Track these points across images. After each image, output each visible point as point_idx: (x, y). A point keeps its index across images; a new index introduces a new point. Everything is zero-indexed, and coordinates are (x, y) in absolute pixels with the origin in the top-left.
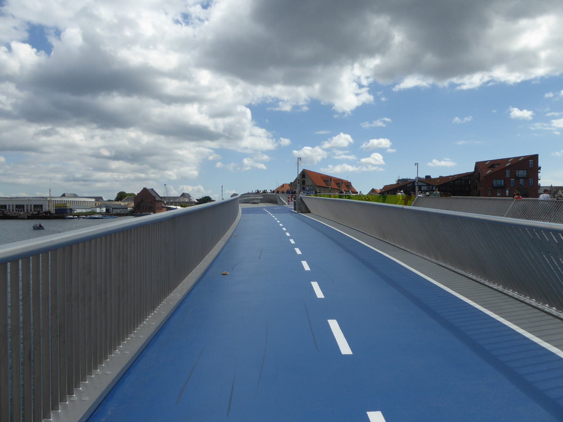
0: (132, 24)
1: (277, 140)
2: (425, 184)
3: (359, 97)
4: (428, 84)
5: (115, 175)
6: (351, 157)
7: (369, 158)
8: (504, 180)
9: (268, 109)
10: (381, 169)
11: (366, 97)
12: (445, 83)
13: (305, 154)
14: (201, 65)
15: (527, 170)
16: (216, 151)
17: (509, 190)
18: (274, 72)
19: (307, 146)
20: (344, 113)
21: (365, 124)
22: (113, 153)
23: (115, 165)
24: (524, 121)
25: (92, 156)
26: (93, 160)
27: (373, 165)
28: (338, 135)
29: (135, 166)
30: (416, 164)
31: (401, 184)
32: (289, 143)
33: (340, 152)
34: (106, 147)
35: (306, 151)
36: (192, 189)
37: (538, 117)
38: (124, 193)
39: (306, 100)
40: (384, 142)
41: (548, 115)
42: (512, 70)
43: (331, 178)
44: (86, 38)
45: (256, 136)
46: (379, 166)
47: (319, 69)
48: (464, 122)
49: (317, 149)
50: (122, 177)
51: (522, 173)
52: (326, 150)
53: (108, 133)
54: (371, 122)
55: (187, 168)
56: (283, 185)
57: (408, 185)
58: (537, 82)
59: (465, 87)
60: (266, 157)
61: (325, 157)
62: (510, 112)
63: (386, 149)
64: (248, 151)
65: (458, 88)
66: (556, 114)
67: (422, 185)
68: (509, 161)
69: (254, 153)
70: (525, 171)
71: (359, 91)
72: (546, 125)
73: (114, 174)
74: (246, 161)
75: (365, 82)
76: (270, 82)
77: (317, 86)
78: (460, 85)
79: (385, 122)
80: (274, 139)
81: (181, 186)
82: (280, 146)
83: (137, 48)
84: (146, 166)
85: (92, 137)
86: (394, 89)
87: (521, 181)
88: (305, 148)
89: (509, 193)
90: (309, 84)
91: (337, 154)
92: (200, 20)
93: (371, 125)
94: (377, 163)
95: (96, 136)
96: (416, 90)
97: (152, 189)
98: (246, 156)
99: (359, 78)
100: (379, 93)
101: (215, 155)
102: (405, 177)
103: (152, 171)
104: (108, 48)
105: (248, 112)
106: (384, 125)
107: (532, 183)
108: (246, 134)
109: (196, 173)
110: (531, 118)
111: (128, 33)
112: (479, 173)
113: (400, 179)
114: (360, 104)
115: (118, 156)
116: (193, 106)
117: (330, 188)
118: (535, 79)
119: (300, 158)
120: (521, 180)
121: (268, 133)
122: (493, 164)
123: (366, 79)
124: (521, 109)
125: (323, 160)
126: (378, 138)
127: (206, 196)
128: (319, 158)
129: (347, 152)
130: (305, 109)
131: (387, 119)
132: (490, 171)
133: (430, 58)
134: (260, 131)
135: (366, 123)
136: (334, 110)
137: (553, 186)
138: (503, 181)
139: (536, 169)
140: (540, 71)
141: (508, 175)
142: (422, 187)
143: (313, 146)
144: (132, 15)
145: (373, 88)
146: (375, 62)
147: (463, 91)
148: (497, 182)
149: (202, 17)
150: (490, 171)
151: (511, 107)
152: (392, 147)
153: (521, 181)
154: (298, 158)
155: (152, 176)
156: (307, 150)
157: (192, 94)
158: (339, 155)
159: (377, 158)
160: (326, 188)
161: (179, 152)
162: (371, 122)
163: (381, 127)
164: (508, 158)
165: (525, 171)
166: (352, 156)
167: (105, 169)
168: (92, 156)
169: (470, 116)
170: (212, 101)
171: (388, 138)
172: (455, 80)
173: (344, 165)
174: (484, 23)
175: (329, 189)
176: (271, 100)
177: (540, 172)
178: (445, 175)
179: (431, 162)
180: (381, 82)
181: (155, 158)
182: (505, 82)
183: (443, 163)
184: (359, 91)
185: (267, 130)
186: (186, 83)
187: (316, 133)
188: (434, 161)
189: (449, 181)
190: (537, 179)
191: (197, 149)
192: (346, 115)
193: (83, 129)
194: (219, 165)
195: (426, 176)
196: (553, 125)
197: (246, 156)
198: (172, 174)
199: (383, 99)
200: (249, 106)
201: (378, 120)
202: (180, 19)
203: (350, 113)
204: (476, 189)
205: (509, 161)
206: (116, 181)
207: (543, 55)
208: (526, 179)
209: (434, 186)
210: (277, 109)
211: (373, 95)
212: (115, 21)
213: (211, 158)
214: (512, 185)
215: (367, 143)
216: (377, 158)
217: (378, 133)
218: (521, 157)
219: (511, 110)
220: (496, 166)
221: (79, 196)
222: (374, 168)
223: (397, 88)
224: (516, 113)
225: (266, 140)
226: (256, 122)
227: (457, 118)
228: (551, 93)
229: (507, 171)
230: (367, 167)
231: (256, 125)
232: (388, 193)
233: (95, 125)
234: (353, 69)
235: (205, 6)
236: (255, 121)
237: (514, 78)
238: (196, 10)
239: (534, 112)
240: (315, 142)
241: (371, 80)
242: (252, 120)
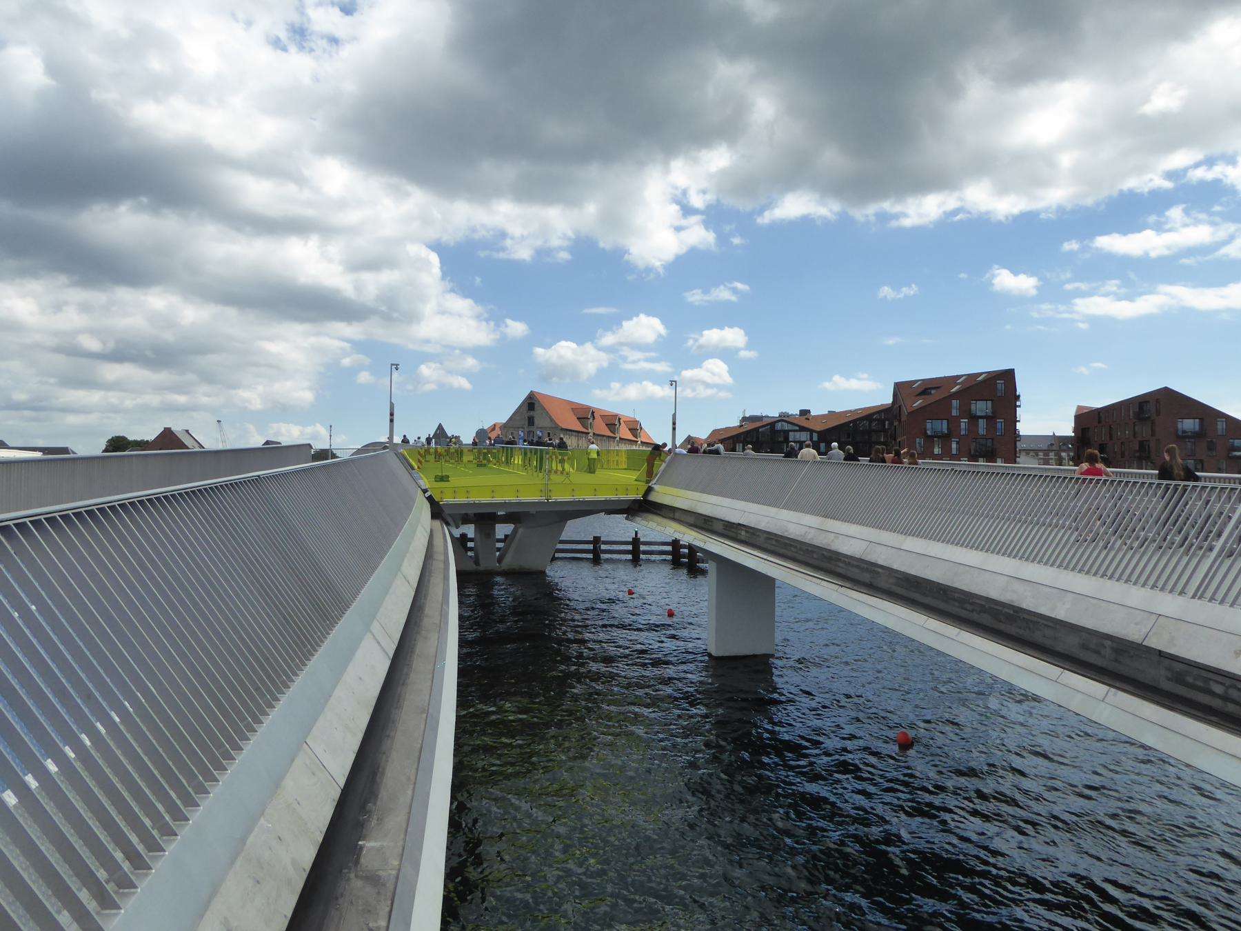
0: (162, 43)
1: (497, 325)
2: (797, 428)
3: (683, 234)
4: (831, 211)
5: (113, 398)
6: (662, 367)
7: (699, 369)
9: (482, 254)
10: (723, 394)
11: (699, 235)
12: (871, 209)
13: (560, 357)
14: (323, 149)
15: (992, 400)
16: (358, 346)
17: (958, 443)
18: (488, 169)
19: (566, 341)
20: (649, 269)
21: (694, 294)
22: (111, 345)
23: (112, 372)
24: (1021, 300)
25: (58, 350)
26: (61, 360)
27: (707, 385)
28: (635, 319)
29: (163, 376)
30: (671, 381)
31: (749, 426)
32: (526, 333)
33: (637, 355)
34: (93, 332)
35: (562, 352)
36: (299, 433)
37: (1049, 292)
38: (124, 438)
39: (565, 237)
40: (733, 336)
41: (1069, 287)
42: (1003, 189)
43: (593, 413)
44: (53, 69)
45: (451, 314)
46: (719, 387)
47: (593, 171)
48: (901, 296)
49: (588, 346)
50: (129, 403)
51: (981, 407)
52: (609, 350)
53: (97, 297)
54: (706, 291)
55: (289, 384)
56: (495, 425)
57: (760, 430)
58: (1050, 215)
59: (907, 223)
60: (470, 362)
61: (605, 364)
62: (994, 276)
63: (737, 350)
64: (430, 349)
65: (894, 224)
66: (1083, 286)
67: (790, 428)
69: (446, 353)
70: (989, 403)
71: (684, 222)
72: (1062, 308)
73: (111, 394)
74: (425, 370)
75: (697, 201)
76: (483, 193)
77: (592, 208)
78: (896, 217)
79: (735, 291)
80: (492, 324)
81: (275, 425)
82: (504, 337)
83: (178, 103)
84: (190, 377)
85: (58, 307)
86: (759, 220)
87: (982, 423)
88: (563, 343)
89: (959, 449)
90: (572, 202)
91: (630, 359)
92: (334, 41)
93: (707, 298)
94: (717, 380)
95: (66, 303)
96: (805, 222)
97: (187, 431)
98: (426, 358)
99: (685, 192)
100: (727, 228)
101: (356, 356)
103: (205, 388)
104: (106, 95)
105: (434, 258)
106: (734, 298)
108: (429, 308)
109: (308, 396)
110: (1034, 292)
111: (156, 64)
112: (900, 407)
114: (682, 250)
115: (121, 353)
116: (306, 242)
117: (591, 434)
118: (1047, 210)
119: (397, 365)
120: (981, 421)
121: (479, 309)
122: (927, 387)
123: (701, 195)
124: (1015, 272)
125: (600, 371)
126: (722, 328)
128: (592, 368)
129: (653, 354)
130: (564, 256)
131: (739, 285)
133: (832, 158)
134: (462, 305)
135: (694, 291)
136: (628, 262)
137: (1056, 434)
138: (945, 422)
139: (1011, 398)
140: (1055, 196)
141: (954, 413)
142: (790, 433)
143: (580, 342)
144: (165, 21)
145: (714, 216)
146: (719, 159)
147: (902, 231)
148: (932, 426)
149: (340, 33)
151: (996, 266)
152: (749, 347)
153: (982, 423)
154: (392, 365)
155: (205, 400)
156: (565, 350)
157: (309, 212)
158: (634, 362)
159: (716, 370)
160: (582, 432)
161: (274, 348)
162: (706, 291)
163: (728, 302)
164: (957, 376)
165: (989, 403)
166: (663, 363)
167: (90, 383)
168: (58, 350)
169: (913, 286)
170: (350, 231)
171: (740, 327)
172: (887, 206)
173: (645, 383)
174: (954, 91)
176: (484, 233)
177: (1020, 406)
178: (838, 409)
179: (830, 379)
180: (730, 202)
181: (211, 358)
182: (988, 213)
183: (854, 384)
184: (684, 222)
185: (476, 301)
186: (291, 188)
187: (586, 311)
188: (836, 378)
189: (847, 421)
190: (1014, 420)
191: (312, 340)
192: (652, 276)
193: (36, 286)
194: (364, 377)
196: (1076, 308)
197: (426, 358)
198: (252, 396)
199: (736, 241)
200: (437, 247)
201: (722, 287)
202: (283, 35)
203: (661, 271)
204: (895, 439)
206: (115, 410)
207: (1066, 160)
208: (990, 419)
210: (502, 255)
211: (714, 232)
212: (125, 33)
213: (346, 362)
214: (963, 433)
215: (696, 336)
216: (716, 369)
217: (721, 316)
218: (982, 374)
219: (997, 272)
220: (933, 392)
221: (11, 446)
222: (709, 392)
223: (766, 218)
224: (1005, 280)
225: (473, 323)
226: (451, 284)
227: (886, 288)
228: (1074, 241)
229: (955, 403)
230: (694, 390)
231: (452, 290)
233: (63, 279)
234: (667, 171)
235: (347, 10)
236: (449, 281)
237: (1005, 206)
238: (325, 19)
239: (1040, 279)
240: (584, 333)
241: (710, 197)
242: (443, 278)
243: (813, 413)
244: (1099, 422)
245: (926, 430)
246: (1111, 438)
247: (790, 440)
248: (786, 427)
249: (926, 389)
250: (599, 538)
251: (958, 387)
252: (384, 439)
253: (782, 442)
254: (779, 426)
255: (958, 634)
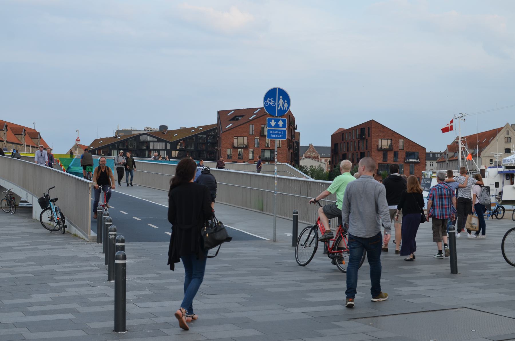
2: (156, 140)
8: (391, 139)
43: (6, 126)
68: (255, 112)
102: (128, 128)
107: (403, 145)
113: (121, 129)
127: (101, 138)
132: (231, 125)
138: (246, 138)
141: (251, 132)
150: (231, 125)
175: (4, 142)
195: (161, 127)
205: (255, 112)
209: (169, 143)
220: (240, 118)
232: (313, 202)
243: (169, 129)
244: (343, 140)
245: (233, 143)
246: (348, 151)
247: (151, 148)
248: (149, 138)
249: (236, 116)
250: (47, 196)
251: (254, 116)
252: (164, 156)
253: (145, 150)
254: (142, 138)
255: (449, 267)
